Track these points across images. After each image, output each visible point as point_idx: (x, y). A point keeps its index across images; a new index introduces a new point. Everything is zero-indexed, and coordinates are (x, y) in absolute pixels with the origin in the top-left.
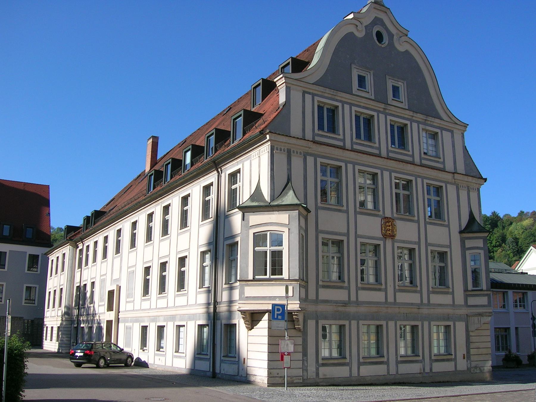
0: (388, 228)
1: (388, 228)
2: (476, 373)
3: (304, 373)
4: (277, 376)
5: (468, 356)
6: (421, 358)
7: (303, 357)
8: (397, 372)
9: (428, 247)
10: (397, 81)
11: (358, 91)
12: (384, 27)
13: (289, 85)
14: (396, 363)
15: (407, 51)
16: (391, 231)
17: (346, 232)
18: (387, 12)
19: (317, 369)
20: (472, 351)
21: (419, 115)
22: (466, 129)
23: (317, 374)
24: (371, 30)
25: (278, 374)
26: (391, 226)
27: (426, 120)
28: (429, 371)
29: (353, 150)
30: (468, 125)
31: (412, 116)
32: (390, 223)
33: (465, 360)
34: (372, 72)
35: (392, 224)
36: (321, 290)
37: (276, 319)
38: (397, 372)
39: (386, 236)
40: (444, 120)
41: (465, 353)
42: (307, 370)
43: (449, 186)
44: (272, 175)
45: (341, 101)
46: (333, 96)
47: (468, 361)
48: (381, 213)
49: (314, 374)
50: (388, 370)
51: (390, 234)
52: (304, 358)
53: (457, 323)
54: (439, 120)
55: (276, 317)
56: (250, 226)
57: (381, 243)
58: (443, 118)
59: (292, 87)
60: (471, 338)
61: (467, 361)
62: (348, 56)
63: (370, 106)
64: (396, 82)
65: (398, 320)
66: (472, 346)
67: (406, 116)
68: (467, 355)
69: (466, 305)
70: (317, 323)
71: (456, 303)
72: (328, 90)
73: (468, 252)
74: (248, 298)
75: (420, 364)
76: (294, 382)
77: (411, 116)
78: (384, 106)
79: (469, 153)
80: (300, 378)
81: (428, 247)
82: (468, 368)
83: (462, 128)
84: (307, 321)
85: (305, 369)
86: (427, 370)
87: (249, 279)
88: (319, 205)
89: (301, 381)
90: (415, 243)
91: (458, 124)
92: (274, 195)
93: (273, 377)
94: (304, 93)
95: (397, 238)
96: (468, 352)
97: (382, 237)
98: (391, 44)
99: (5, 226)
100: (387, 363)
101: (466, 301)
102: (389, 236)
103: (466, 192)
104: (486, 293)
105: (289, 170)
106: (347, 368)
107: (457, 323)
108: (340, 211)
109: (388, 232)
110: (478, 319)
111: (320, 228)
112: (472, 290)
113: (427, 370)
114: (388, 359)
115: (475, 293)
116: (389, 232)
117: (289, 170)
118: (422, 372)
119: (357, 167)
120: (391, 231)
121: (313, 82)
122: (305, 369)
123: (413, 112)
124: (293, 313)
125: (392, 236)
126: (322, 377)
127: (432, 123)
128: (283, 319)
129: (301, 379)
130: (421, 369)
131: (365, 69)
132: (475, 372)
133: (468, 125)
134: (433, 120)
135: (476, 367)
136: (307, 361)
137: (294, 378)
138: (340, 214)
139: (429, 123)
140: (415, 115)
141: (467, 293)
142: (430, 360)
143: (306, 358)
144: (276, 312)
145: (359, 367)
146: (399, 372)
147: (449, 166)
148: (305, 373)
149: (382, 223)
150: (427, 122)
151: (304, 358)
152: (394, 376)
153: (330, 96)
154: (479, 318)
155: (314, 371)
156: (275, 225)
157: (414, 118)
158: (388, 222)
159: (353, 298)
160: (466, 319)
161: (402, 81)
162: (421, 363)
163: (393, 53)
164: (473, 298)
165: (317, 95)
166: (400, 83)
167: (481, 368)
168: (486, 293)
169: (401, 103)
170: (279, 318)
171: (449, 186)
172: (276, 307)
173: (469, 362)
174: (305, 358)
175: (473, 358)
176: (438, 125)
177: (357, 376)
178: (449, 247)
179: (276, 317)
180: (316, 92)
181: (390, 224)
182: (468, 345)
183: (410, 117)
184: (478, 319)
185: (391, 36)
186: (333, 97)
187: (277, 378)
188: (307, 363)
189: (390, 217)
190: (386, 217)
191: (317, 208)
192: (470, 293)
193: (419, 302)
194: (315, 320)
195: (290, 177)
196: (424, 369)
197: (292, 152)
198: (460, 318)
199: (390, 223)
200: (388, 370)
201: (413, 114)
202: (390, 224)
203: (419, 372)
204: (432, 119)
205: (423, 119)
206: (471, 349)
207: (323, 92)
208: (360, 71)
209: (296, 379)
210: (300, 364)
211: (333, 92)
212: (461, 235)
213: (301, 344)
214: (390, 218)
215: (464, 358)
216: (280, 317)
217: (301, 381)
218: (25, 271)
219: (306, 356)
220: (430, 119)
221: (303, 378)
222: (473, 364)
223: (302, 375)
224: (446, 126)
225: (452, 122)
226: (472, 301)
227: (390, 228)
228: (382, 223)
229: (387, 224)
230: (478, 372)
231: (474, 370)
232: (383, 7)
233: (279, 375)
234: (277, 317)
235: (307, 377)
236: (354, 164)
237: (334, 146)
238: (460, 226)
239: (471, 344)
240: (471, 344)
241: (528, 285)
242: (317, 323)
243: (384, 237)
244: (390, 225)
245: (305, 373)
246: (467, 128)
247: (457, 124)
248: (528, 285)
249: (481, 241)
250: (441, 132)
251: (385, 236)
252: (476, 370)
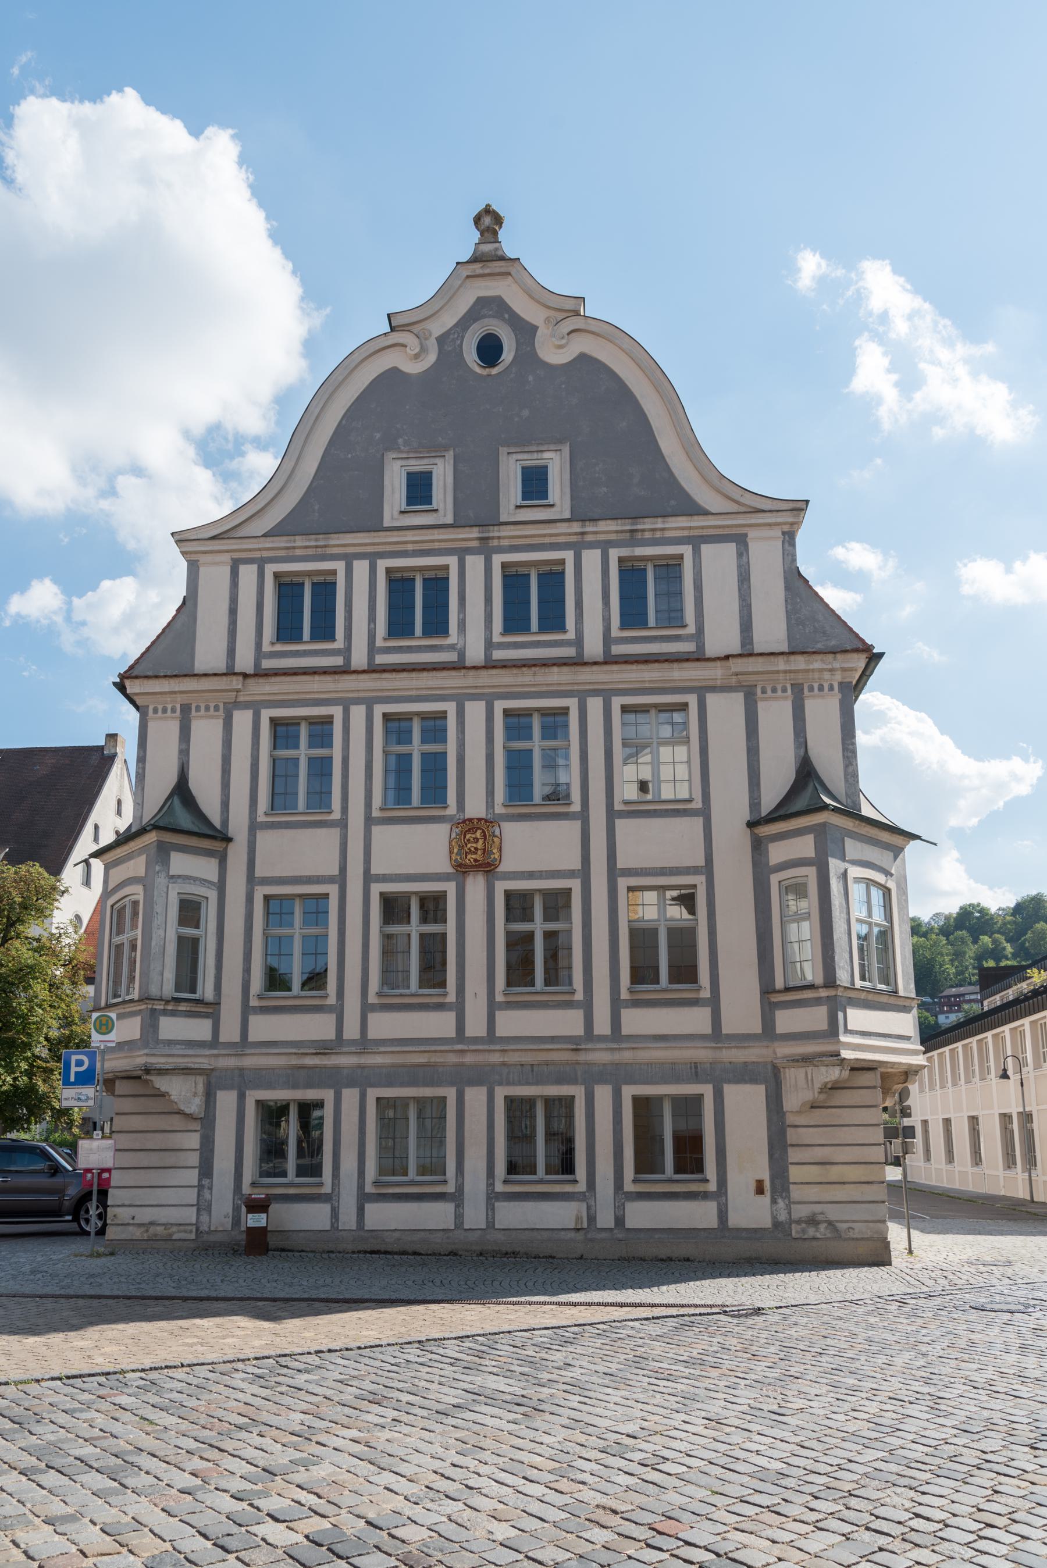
2: (814, 1239)
4: (131, 1222)
7: (200, 1180)
12: (506, 316)
13: (194, 557)
16: (479, 852)
17: (336, 872)
20: (795, 1173)
21: (603, 526)
25: (133, 1218)
26: (481, 842)
27: (632, 531)
31: (583, 534)
32: (479, 832)
33: (766, 1199)
35: (485, 835)
36: (254, 1020)
38: (491, 1223)
39: (466, 866)
41: (766, 1176)
42: (209, 1209)
44: (140, 771)
46: (320, 549)
47: (780, 1201)
48: (452, 810)
49: (227, 1219)
50: (459, 1217)
51: (476, 860)
52: (203, 1182)
54: (701, 518)
58: (707, 507)
59: (202, 559)
60: (789, 1131)
61: (774, 1201)
63: (436, 545)
64: (535, 456)
66: (793, 1155)
67: (561, 539)
70: (242, 1097)
71: (725, 1030)
72: (300, 541)
76: (174, 1237)
77: (576, 534)
78: (479, 532)
80: (190, 1228)
82: (776, 1224)
83: (788, 518)
84: (215, 1094)
85: (203, 1206)
86: (605, 1219)
89: (193, 1236)
93: (122, 1225)
100: (457, 1198)
102: (472, 866)
105: (184, 753)
113: (605, 1219)
117: (184, 753)
118: (585, 1225)
119: (617, 702)
120: (479, 852)
122: (203, 1206)
123: (580, 523)
125: (488, 868)
127: (658, 535)
129: (191, 1231)
130: (578, 1219)
131: (428, 452)
132: (806, 1237)
134: (660, 526)
135: (812, 1221)
136: (211, 1188)
137: (174, 1229)
139: (647, 535)
140: (590, 528)
142: (615, 1193)
149: (454, 835)
150: (639, 536)
151: (203, 1182)
153: (310, 552)
157: (589, 538)
158: (472, 830)
161: (552, 447)
162: (584, 1200)
163: (531, 378)
166: (546, 455)
173: (781, 1204)
174: (206, 1182)
175: (796, 1193)
176: (685, 533)
177: (354, 1228)
178: (704, 870)
180: (265, 554)
181: (478, 834)
183: (574, 539)
185: (525, 331)
186: (320, 551)
187: (131, 1228)
188: (211, 1194)
196: (592, 1219)
197: (759, 690)
199: (479, 832)
201: (583, 526)
204: (656, 523)
205: (622, 532)
207: (287, 548)
209: (179, 1232)
210: (191, 1196)
211: (317, 540)
213: (198, 1147)
215: (760, 1190)
217: (193, 1236)
220: (647, 524)
222: (801, 1212)
224: (719, 527)
225: (742, 509)
228: (452, 837)
229: (468, 837)
232: (502, 263)
233: (136, 1221)
235: (209, 1227)
236: (606, 695)
237: (314, 670)
242: (242, 1097)
245: (205, 1218)
251: (462, 870)
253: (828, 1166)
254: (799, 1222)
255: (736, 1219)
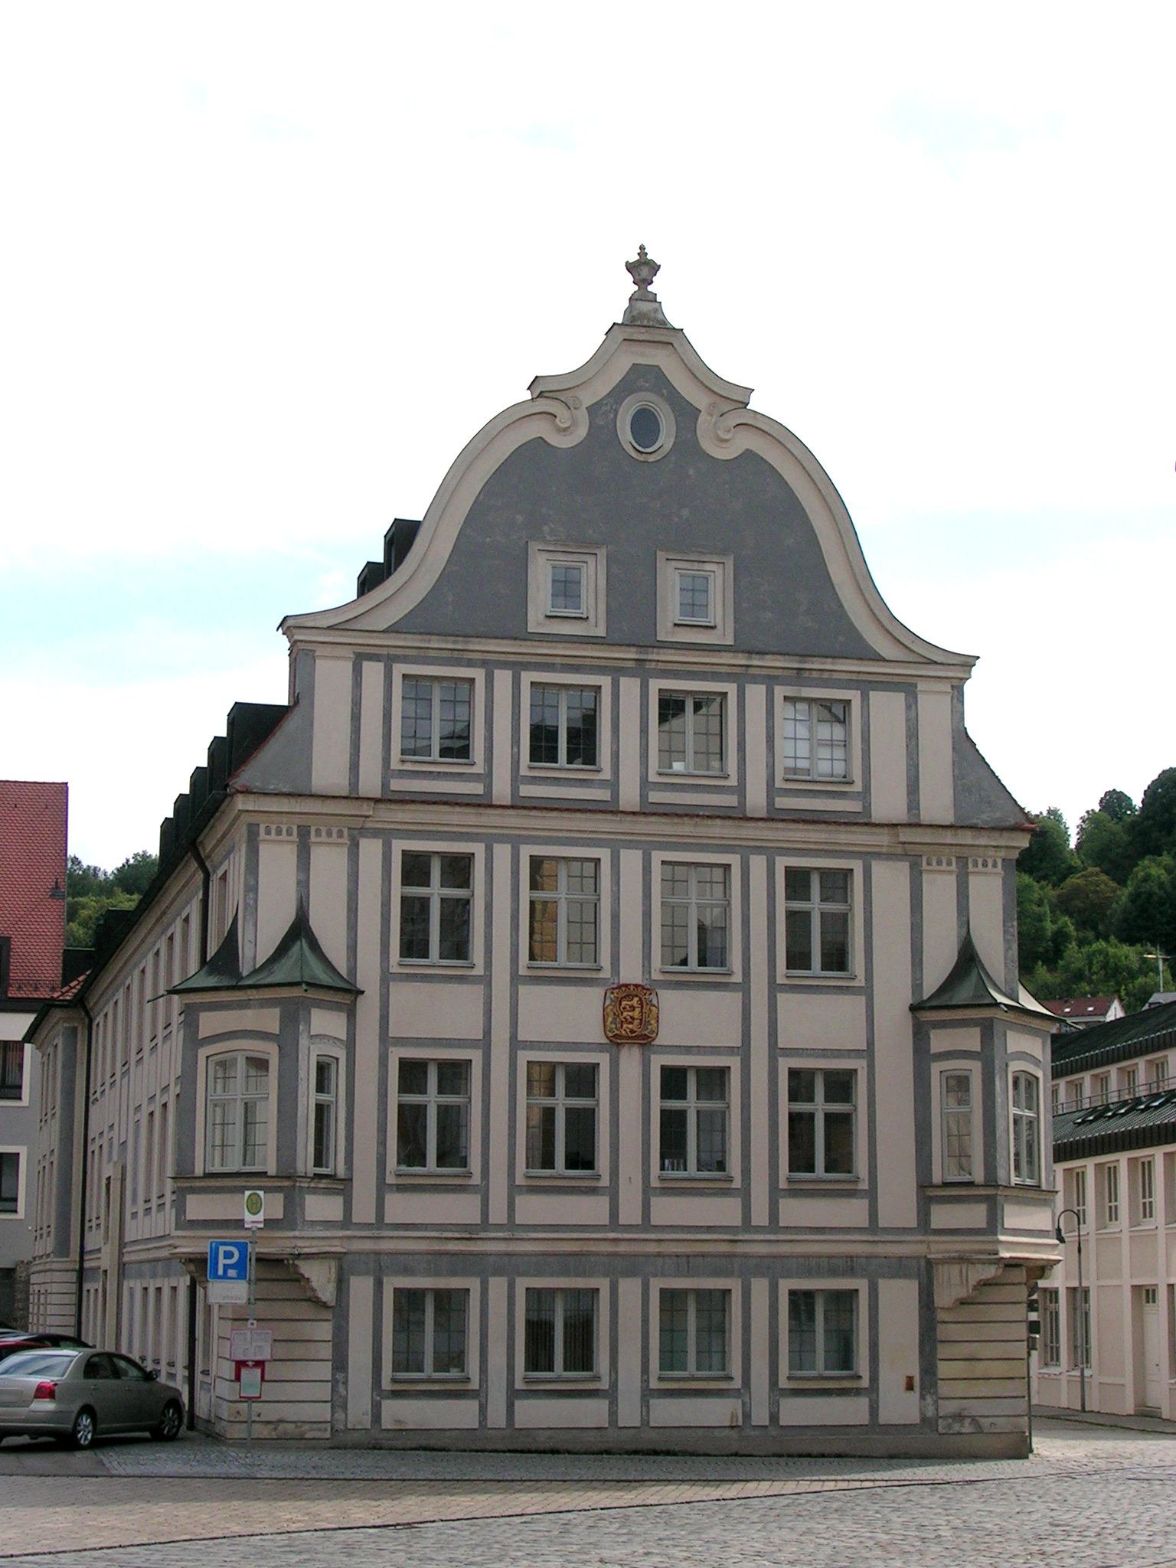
0: (625, 1014)
1: (625, 1014)
4: (258, 1419)
6: (737, 1384)
8: (645, 1421)
10: (699, 562)
11: (548, 621)
15: (748, 454)
16: (636, 1022)
18: (675, 345)
19: (376, 1408)
20: (944, 1369)
23: (377, 1417)
25: (259, 1416)
26: (637, 1010)
29: (519, 805)
32: (636, 999)
33: (915, 1395)
34: (602, 553)
37: (220, 1277)
38: (645, 1421)
41: (916, 1373)
42: (345, 1408)
43: (879, 869)
45: (484, 664)
48: (606, 973)
49: (366, 1417)
50: (613, 1414)
51: (632, 1031)
55: (220, 1272)
57: (603, 1060)
60: (940, 1328)
61: (922, 1397)
62: (520, 518)
64: (696, 566)
65: (655, 1276)
66: (943, 1351)
68: (921, 1379)
70: (379, 1285)
73: (936, 1068)
74: (194, 1224)
75: (735, 1400)
76: (307, 1436)
80: (324, 1425)
82: (924, 1419)
84: (349, 1280)
85: (339, 1402)
88: (394, 969)
89: (328, 1435)
90: (730, 1051)
92: (255, 957)
94: (359, 659)
95: (661, 1040)
96: (928, 1368)
98: (687, 446)
99: (520, 973)
100: (611, 1394)
103: (951, 881)
104: (982, 1192)
105: (304, 885)
106: (473, 1405)
108: (462, 979)
109: (625, 1026)
110: (961, 1271)
111: (393, 1032)
113: (760, 1416)
115: (953, 1193)
116: (630, 1026)
117: (304, 885)
120: (636, 1022)
121: (385, 627)
125: (644, 1040)
126: (389, 1427)
128: (242, 1276)
130: (733, 1416)
132: (951, 1432)
133: (978, 658)
135: (959, 1417)
136: (345, 1383)
137: (306, 1427)
138: (465, 988)
143: (343, 1375)
144: (222, 1261)
145: (513, 1405)
146: (651, 1420)
147: (888, 804)
148: (340, 1415)
149: (608, 1002)
152: (633, 1431)
154: (964, 1267)
158: (630, 997)
159: (498, 1215)
164: (948, 1207)
165: (405, 659)
167: (982, 1420)
168: (982, 1192)
169: (710, 631)
170: (229, 1275)
171: (879, 869)
172: (222, 1249)
174: (340, 1376)
175: (944, 1389)
179: (220, 1272)
182: (927, 1349)
184: (961, 1271)
192: (198, 1184)
193: (476, 1219)
194: (372, 1279)
195: (305, 904)
196: (747, 1416)
198: (898, 1268)
199: (636, 999)
200: (613, 1414)
206: (939, 1362)
208: (562, 557)
210: (325, 1391)
214: (636, 986)
215: (910, 1387)
216: (232, 1273)
217: (328, 1435)
221: (332, 1428)
222: (948, 1407)
223: (329, 1420)
230: (964, 1430)
231: (949, 1426)
233: (262, 1419)
234: (225, 1271)
238: (917, 986)
239: (939, 1345)
240: (939, 1345)
242: (379, 1285)
243: (611, 1041)
244: (635, 1005)
247: (936, 663)
249: (976, 1033)
250: (865, 699)
251: (616, 1042)
252: (956, 1427)
253: (973, 1362)
254: (944, 1417)
255: (886, 1416)
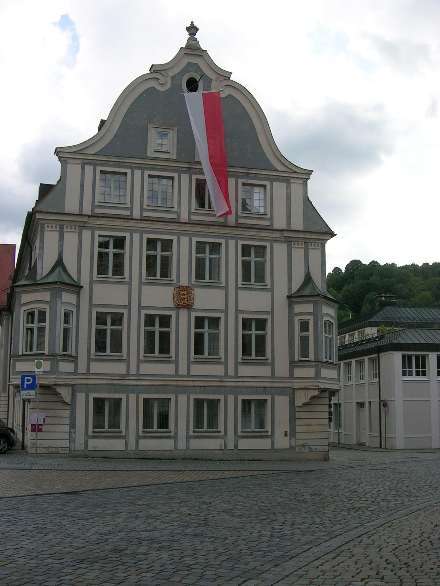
3: (71, 445)
4: (41, 446)
5: (292, 433)
9: (239, 314)
14: (187, 438)
18: (203, 56)
19: (86, 442)
20: (298, 429)
22: (310, 176)
23: (86, 446)
24: (180, 80)
25: (42, 445)
28: (233, 448)
29: (143, 219)
30: (313, 171)
32: (186, 291)
34: (175, 129)
38: (188, 448)
40: (279, 171)
42: (74, 442)
48: (175, 282)
50: (176, 445)
51: (184, 303)
53: (277, 398)
56: (22, 303)
57: (173, 314)
61: (290, 439)
66: (298, 422)
69: (291, 376)
70: (87, 396)
76: (60, 453)
79: (312, 205)
81: (239, 314)
82: (291, 447)
85: (72, 440)
87: (19, 355)
88: (95, 278)
89: (68, 452)
91: (298, 172)
97: (175, 307)
101: (291, 372)
107: (277, 398)
109: (181, 301)
112: (300, 361)
114: (176, 434)
124: (51, 387)
125: (189, 307)
129: (67, 450)
130: (221, 446)
133: (313, 171)
135: (303, 446)
137: (60, 449)
138: (121, 286)
141: (293, 364)
143: (74, 430)
149: (175, 292)
155: (83, 443)
156: (40, 303)
158: (183, 290)
160: (292, 392)
171: (276, 246)
173: (293, 439)
174: (72, 430)
175: (298, 436)
184: (305, 393)
189: (187, 285)
190: (181, 286)
191: (92, 282)
195: (61, 254)
196: (226, 446)
198: (282, 391)
202: (185, 292)
203: (219, 449)
209: (62, 450)
210: (67, 436)
212: (290, 299)
214: (186, 287)
215: (286, 435)
218: (94, 392)
219: (74, 429)
221: (69, 450)
223: (68, 447)
226: (298, 372)
227: (186, 297)
229: (181, 293)
233: (43, 446)
238: (290, 289)
241: (43, 334)
242: (87, 396)
245: (72, 445)
246: (311, 175)
247: (298, 173)
248: (43, 334)
249: (311, 306)
251: (178, 307)
253: (309, 426)
